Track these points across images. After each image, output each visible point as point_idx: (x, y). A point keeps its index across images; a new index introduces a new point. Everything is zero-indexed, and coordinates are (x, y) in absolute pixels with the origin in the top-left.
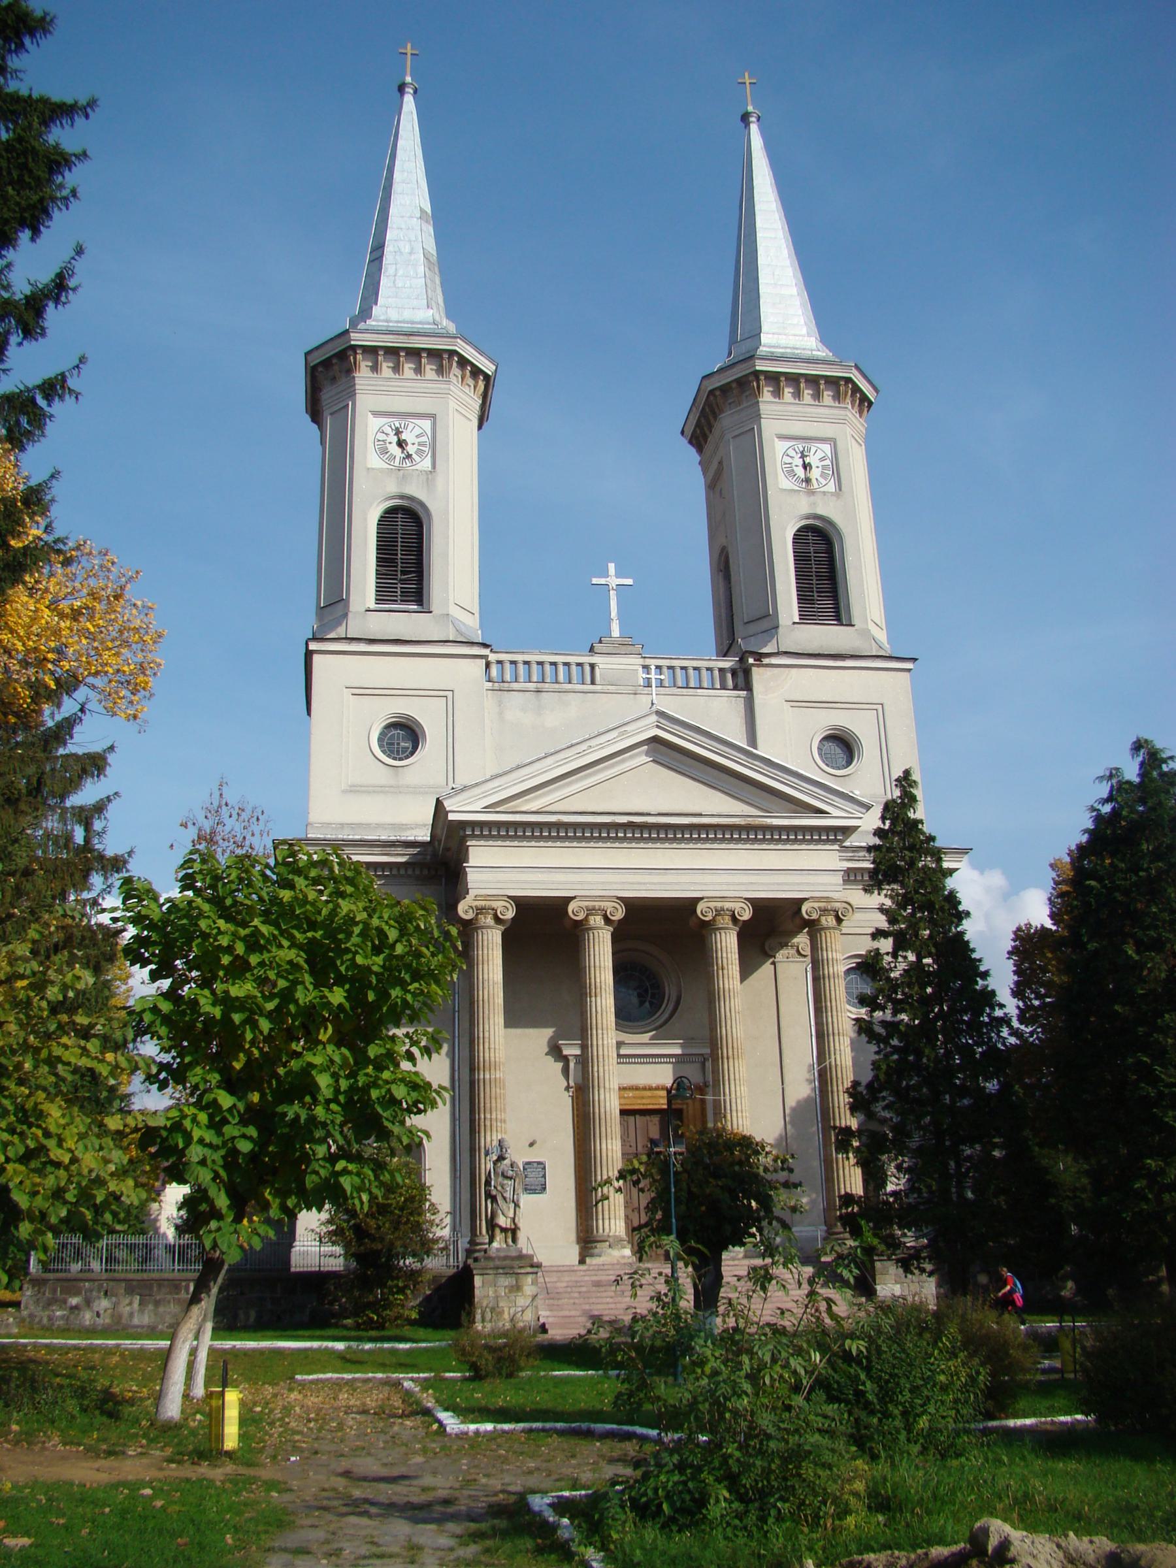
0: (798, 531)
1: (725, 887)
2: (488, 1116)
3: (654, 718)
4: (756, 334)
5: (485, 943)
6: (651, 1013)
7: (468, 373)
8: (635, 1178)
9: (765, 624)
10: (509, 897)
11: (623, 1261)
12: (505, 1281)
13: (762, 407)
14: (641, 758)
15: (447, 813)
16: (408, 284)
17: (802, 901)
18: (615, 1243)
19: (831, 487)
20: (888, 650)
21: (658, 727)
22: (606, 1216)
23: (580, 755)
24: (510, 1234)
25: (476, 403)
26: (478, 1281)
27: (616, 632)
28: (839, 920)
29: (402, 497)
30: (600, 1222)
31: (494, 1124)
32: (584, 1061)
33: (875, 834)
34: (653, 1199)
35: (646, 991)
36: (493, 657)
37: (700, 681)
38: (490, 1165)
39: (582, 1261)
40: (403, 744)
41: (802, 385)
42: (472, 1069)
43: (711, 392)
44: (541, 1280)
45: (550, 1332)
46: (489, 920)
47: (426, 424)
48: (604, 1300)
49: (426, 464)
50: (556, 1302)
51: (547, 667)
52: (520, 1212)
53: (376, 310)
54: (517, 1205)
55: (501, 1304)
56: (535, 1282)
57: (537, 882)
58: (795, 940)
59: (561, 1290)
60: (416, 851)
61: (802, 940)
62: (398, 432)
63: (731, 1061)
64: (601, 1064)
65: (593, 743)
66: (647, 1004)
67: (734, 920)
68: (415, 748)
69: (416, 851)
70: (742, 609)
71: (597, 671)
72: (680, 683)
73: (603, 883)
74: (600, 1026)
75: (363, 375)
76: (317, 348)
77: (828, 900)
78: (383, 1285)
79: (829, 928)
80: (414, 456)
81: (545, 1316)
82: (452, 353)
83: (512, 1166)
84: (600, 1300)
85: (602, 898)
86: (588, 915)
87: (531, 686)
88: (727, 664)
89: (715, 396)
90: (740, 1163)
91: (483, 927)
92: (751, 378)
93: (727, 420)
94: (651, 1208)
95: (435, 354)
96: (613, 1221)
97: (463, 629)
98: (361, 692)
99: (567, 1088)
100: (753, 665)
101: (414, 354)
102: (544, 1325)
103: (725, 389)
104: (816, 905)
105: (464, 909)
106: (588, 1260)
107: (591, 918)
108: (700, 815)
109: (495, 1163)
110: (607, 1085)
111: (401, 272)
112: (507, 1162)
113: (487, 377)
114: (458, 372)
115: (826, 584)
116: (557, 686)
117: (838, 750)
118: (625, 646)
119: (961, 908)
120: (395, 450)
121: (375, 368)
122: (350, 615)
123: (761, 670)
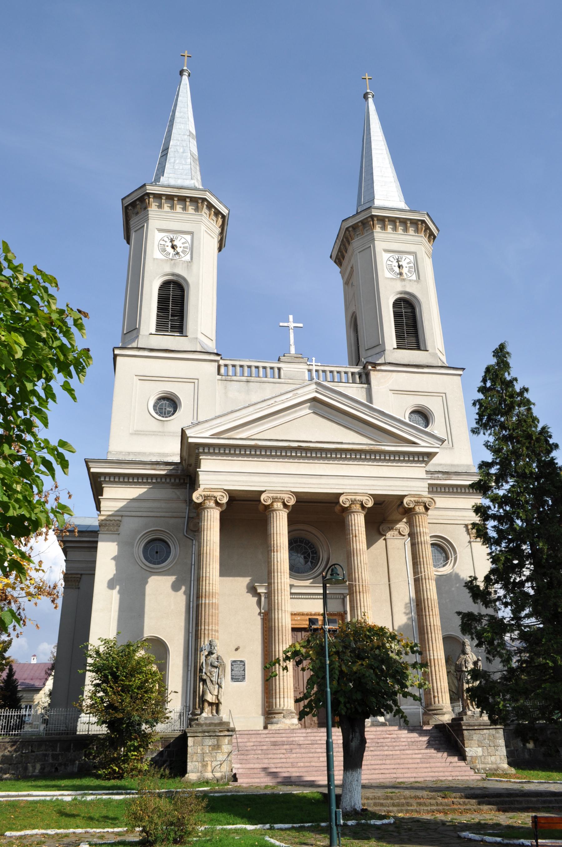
0: (396, 300)
1: (356, 487)
2: (207, 627)
3: (314, 387)
4: (372, 200)
5: (209, 517)
6: (312, 569)
7: (213, 213)
8: (297, 659)
9: (377, 350)
10: (225, 490)
11: (292, 727)
12: (209, 742)
13: (375, 234)
14: (305, 410)
15: (188, 438)
16: (181, 168)
17: (404, 496)
18: (287, 714)
19: (414, 277)
20: (447, 365)
21: (316, 392)
22: (282, 696)
23: (270, 406)
24: (214, 707)
25: (218, 230)
26: (190, 741)
27: (293, 350)
28: (427, 509)
29: (173, 275)
30: (278, 700)
31: (210, 632)
32: (269, 595)
33: (479, 391)
34: (312, 676)
35: (309, 555)
36: (222, 362)
37: (341, 379)
38: (203, 659)
39: (265, 728)
40: (168, 409)
41: (398, 224)
42: (198, 597)
43: (347, 229)
44: (234, 741)
45: (239, 780)
46: (212, 504)
47: (188, 237)
48: (278, 756)
49: (188, 258)
50: (245, 757)
51: (253, 369)
52: (222, 691)
53: (162, 179)
54: (220, 686)
55: (206, 759)
56: (230, 743)
57: (243, 482)
58: (398, 526)
59: (249, 748)
60: (171, 467)
61: (403, 526)
62: (172, 241)
63: (361, 594)
64: (280, 595)
65: (277, 399)
66: (309, 563)
67: (363, 507)
68: (175, 411)
69: (171, 467)
70: (365, 343)
71: (282, 372)
72: (329, 379)
73: (282, 483)
74: (279, 570)
75: (153, 209)
76: (128, 196)
77: (420, 496)
78: (124, 745)
79: (420, 513)
80: (181, 253)
81: (237, 768)
82: (204, 200)
83: (218, 659)
84: (276, 756)
85: (281, 492)
86: (273, 502)
87: (244, 378)
88: (356, 370)
89: (349, 231)
90: (378, 647)
91: (208, 508)
92: (370, 219)
93: (356, 243)
94: (310, 682)
95: (194, 200)
96: (286, 699)
97: (205, 347)
98: (144, 378)
99: (260, 613)
100: (371, 370)
101: (182, 199)
102: (235, 774)
103: (354, 227)
104: (412, 499)
105: (196, 497)
106: (269, 726)
107: (275, 504)
108: (342, 443)
109: (206, 657)
110: (283, 609)
111: (177, 162)
112: (214, 656)
113: (223, 217)
114: (207, 212)
115: (412, 330)
116: (258, 379)
117: (420, 419)
118: (299, 358)
119: (551, 441)
120: (171, 251)
121: (160, 206)
122: (140, 337)
123: (376, 373)
